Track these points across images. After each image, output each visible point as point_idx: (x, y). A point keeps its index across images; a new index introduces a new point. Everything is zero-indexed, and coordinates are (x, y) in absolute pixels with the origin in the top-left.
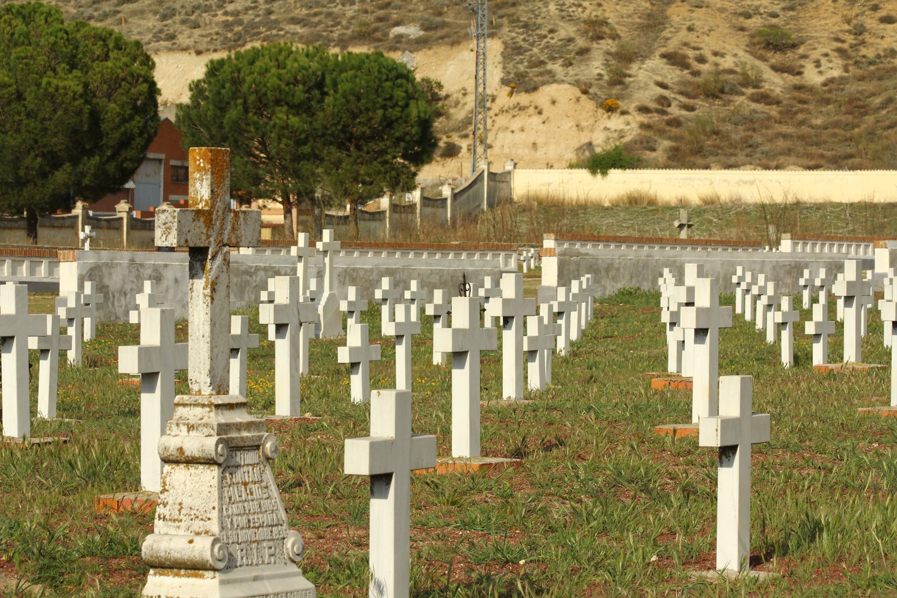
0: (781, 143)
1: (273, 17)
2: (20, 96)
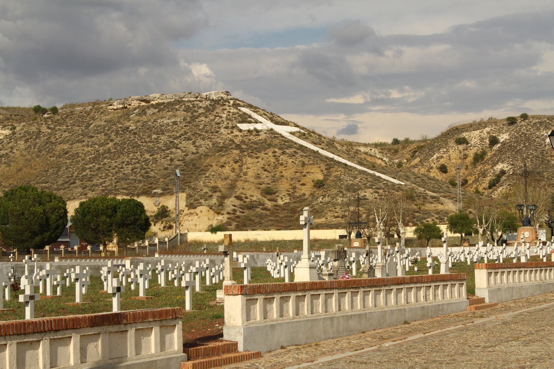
0: (270, 223)
1: (117, 188)
2: (23, 214)
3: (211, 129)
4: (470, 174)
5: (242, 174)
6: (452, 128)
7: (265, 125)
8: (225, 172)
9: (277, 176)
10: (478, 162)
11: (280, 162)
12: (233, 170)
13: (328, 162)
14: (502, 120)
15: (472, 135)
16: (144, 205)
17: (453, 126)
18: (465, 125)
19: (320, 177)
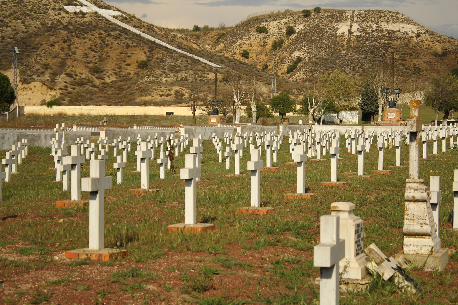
0: (100, 99)
3: (39, 10)
4: (270, 60)
5: (70, 53)
6: (252, 18)
7: (90, 8)
8: (54, 50)
9: (103, 56)
10: (276, 49)
11: (106, 43)
12: (62, 49)
13: (150, 45)
14: (297, 12)
15: (271, 25)
16: (9, 78)
17: (252, 16)
18: (264, 16)
19: (144, 58)
